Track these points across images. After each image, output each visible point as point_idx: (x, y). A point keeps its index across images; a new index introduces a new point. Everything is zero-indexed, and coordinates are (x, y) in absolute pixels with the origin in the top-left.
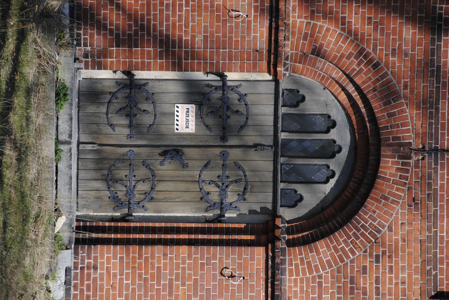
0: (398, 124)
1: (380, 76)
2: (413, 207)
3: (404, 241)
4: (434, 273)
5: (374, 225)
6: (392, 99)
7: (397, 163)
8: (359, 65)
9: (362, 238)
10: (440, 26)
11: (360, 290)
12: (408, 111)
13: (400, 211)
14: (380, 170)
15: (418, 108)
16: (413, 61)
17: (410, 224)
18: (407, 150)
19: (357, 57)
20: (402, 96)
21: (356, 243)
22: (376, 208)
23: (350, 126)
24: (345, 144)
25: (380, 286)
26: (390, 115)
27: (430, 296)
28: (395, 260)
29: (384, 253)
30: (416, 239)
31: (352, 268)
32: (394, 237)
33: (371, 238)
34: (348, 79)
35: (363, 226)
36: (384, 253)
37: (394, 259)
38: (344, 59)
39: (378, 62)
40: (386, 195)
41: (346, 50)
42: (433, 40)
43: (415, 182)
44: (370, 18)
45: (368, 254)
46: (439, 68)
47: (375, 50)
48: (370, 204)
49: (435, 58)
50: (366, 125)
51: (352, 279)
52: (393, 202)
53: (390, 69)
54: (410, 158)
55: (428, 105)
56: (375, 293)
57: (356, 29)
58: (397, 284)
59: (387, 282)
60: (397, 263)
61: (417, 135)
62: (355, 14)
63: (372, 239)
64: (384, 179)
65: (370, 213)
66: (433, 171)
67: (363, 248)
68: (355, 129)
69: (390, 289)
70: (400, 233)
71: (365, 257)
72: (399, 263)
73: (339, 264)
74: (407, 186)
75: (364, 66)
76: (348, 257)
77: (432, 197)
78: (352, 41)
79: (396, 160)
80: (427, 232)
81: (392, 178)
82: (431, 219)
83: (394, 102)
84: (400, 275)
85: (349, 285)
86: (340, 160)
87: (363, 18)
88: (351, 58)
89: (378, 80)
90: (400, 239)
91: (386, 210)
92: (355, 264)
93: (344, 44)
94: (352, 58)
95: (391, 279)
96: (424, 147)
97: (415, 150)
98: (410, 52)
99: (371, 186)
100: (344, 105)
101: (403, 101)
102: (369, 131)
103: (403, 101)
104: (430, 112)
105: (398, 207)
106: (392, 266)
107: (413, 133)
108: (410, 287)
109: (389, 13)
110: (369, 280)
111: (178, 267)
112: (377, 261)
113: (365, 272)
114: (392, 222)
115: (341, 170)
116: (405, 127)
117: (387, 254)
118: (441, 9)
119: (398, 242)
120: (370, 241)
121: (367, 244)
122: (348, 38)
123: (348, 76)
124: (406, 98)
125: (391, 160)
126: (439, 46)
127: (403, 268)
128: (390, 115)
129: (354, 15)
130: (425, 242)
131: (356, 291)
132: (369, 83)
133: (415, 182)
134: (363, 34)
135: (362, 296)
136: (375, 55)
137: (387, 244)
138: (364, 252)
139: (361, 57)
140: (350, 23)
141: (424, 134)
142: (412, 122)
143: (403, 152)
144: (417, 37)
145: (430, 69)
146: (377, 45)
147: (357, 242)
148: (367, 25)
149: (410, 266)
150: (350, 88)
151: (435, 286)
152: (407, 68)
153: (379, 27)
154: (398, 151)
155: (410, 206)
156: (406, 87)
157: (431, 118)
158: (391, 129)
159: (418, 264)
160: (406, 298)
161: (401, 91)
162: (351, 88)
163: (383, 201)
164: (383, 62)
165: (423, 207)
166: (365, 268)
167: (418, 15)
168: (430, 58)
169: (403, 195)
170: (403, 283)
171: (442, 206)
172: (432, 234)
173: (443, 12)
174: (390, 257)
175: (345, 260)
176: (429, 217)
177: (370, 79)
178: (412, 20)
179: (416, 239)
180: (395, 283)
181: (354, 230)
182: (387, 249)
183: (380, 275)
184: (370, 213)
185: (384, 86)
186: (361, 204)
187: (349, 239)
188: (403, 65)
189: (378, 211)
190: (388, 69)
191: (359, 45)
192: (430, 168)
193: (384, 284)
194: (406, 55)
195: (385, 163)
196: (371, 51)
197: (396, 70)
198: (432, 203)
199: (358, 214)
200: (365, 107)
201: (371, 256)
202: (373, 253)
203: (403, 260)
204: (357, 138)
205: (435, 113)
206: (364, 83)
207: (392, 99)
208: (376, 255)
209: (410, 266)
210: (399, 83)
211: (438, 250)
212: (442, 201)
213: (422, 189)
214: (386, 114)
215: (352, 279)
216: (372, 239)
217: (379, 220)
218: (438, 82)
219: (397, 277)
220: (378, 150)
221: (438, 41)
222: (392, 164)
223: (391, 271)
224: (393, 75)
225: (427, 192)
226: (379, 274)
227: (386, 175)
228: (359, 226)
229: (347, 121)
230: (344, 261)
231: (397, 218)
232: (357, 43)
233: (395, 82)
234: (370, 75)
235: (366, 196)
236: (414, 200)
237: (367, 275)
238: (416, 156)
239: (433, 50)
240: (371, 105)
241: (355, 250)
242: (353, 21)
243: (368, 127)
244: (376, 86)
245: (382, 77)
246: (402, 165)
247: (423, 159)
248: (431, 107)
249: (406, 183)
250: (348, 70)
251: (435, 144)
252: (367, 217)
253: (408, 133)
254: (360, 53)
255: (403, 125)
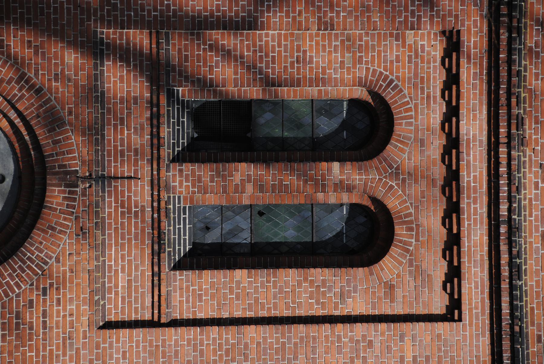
0: (64, 151)
1: (43, 102)
2: (81, 237)
3: (72, 272)
4: (102, 303)
5: (40, 257)
6: (57, 126)
7: (64, 192)
8: (20, 90)
9: (28, 271)
10: (102, 51)
11: (26, 325)
12: (73, 137)
13: (67, 241)
14: (46, 199)
15: (84, 135)
16: (76, 86)
17: (78, 254)
18: (74, 178)
19: (17, 82)
20: (67, 122)
21: (22, 277)
22: (43, 239)
23: (13, 154)
24: (8, 174)
25: (47, 319)
26: (55, 142)
27: (98, 327)
28: (63, 292)
29: (51, 285)
30: (84, 269)
31: (18, 302)
32: (61, 269)
33: (38, 270)
34: (10, 105)
35: (29, 259)
36: (51, 285)
37: (62, 291)
38: (5, 84)
39: (40, 87)
40: (53, 225)
41: (6, 75)
42: (96, 65)
43: (82, 210)
44: (29, 42)
45: (34, 287)
46: (103, 93)
47: (36, 74)
48: (37, 235)
49: (99, 83)
50: (30, 153)
51: (18, 313)
52: (60, 232)
53: (54, 95)
54: (77, 186)
55: (94, 132)
56: (42, 327)
57: (16, 53)
58: (64, 316)
59: (55, 315)
60: (65, 295)
61: (83, 162)
62: (14, 37)
63: (39, 271)
64: (50, 208)
65: (37, 245)
66: (100, 199)
67: (29, 282)
68: (18, 157)
69: (58, 322)
70: (68, 263)
71: (31, 290)
72: (67, 295)
73: (3, 299)
74: (74, 215)
75: (26, 91)
76: (13, 292)
77: (100, 225)
78: (12, 66)
79: (63, 188)
80: (95, 262)
81: (59, 208)
82: (99, 248)
83: (59, 129)
84: (68, 307)
85: (15, 321)
86: (3, 190)
87: (22, 42)
88: (11, 83)
89: (41, 106)
90: (68, 270)
91: (53, 241)
92: (21, 299)
93: (4, 69)
94: (13, 83)
95: (58, 312)
96: (90, 175)
97: (82, 178)
98: (73, 77)
99: (37, 216)
100: (7, 133)
101: (68, 127)
102: (34, 159)
103: (68, 127)
104: (95, 139)
105: (66, 237)
106: (60, 298)
107: (79, 161)
108: (78, 319)
109: (49, 36)
110: (36, 314)
111: (98, 347)
112: (45, 294)
113: (31, 306)
114: (59, 253)
115: (5, 201)
116: (70, 154)
117: (55, 286)
118: (102, 33)
119: (66, 273)
120: (36, 274)
121: (34, 276)
122: (8, 62)
123: (9, 102)
124: (71, 124)
125: (57, 189)
126: (102, 72)
127: (71, 299)
128: (55, 142)
129: (12, 38)
130: (93, 272)
131: (22, 326)
132: (32, 109)
133: (82, 210)
134: (23, 58)
135: (28, 331)
136: (37, 80)
137: (55, 275)
138: (30, 286)
139: (22, 82)
140: (9, 46)
141: (90, 161)
142: (78, 149)
143: (70, 180)
144: (80, 62)
145: (94, 95)
146: (39, 70)
147: (23, 275)
148: (28, 49)
149: (78, 297)
150: (11, 115)
151: (104, 316)
152: (71, 94)
153: (40, 50)
154: (64, 179)
155: (77, 235)
156: (70, 113)
157: (97, 144)
158: (57, 156)
159: (87, 294)
160: (74, 330)
161: (65, 117)
162: (13, 115)
163: (50, 231)
164: (45, 87)
165: (90, 236)
166: (31, 301)
167: (79, 39)
168: (94, 83)
169: (70, 224)
170: (71, 315)
171: (110, 235)
172: (100, 264)
173: (104, 36)
174: (58, 289)
175: (11, 294)
176: (97, 247)
177: (32, 105)
178: (73, 44)
179: (84, 269)
180: (63, 315)
181: (20, 263)
182: (54, 281)
183: (48, 308)
184: (37, 245)
185: (48, 112)
186: (27, 235)
187: (14, 273)
188: (66, 90)
189: (45, 243)
190: (52, 95)
191: (20, 70)
192: (97, 195)
193: (51, 317)
194: (69, 80)
195: (51, 192)
196: (32, 76)
197: (60, 95)
198: (100, 231)
199: (23, 246)
200: (28, 134)
201: (38, 289)
202: (40, 286)
203: (71, 291)
204: (21, 167)
205: (101, 140)
206: (27, 109)
207: (57, 126)
208: (43, 288)
209: (78, 297)
210: (63, 108)
211: (106, 280)
212: (110, 229)
213: (90, 218)
214: (50, 141)
215: (18, 313)
216: (39, 271)
217: (46, 251)
218: (103, 108)
219: (65, 310)
220: (44, 179)
221: (101, 66)
222: (58, 193)
223: (58, 304)
224: (56, 101)
225: (95, 221)
226: (46, 307)
227: (52, 204)
228: (25, 259)
229: (9, 149)
230: (9, 296)
231: (64, 249)
232: (17, 68)
233: (59, 108)
234: (33, 101)
235: (32, 226)
236: (82, 229)
237: (34, 309)
238: (83, 184)
239: (96, 75)
240: (35, 133)
241: (21, 284)
242: (12, 44)
243: (33, 155)
244: (40, 113)
245: (46, 103)
246: (69, 194)
247: (90, 187)
248: (97, 134)
249: (73, 212)
250: (9, 95)
251: (101, 171)
252: (33, 249)
253: (74, 161)
254: (22, 77)
255: (69, 152)
